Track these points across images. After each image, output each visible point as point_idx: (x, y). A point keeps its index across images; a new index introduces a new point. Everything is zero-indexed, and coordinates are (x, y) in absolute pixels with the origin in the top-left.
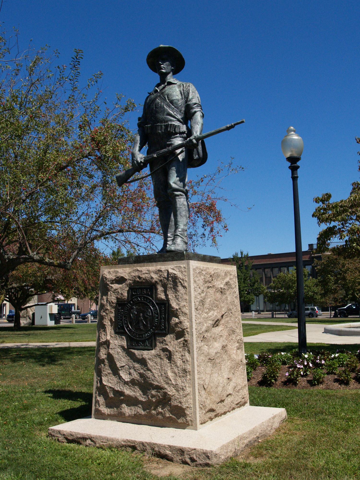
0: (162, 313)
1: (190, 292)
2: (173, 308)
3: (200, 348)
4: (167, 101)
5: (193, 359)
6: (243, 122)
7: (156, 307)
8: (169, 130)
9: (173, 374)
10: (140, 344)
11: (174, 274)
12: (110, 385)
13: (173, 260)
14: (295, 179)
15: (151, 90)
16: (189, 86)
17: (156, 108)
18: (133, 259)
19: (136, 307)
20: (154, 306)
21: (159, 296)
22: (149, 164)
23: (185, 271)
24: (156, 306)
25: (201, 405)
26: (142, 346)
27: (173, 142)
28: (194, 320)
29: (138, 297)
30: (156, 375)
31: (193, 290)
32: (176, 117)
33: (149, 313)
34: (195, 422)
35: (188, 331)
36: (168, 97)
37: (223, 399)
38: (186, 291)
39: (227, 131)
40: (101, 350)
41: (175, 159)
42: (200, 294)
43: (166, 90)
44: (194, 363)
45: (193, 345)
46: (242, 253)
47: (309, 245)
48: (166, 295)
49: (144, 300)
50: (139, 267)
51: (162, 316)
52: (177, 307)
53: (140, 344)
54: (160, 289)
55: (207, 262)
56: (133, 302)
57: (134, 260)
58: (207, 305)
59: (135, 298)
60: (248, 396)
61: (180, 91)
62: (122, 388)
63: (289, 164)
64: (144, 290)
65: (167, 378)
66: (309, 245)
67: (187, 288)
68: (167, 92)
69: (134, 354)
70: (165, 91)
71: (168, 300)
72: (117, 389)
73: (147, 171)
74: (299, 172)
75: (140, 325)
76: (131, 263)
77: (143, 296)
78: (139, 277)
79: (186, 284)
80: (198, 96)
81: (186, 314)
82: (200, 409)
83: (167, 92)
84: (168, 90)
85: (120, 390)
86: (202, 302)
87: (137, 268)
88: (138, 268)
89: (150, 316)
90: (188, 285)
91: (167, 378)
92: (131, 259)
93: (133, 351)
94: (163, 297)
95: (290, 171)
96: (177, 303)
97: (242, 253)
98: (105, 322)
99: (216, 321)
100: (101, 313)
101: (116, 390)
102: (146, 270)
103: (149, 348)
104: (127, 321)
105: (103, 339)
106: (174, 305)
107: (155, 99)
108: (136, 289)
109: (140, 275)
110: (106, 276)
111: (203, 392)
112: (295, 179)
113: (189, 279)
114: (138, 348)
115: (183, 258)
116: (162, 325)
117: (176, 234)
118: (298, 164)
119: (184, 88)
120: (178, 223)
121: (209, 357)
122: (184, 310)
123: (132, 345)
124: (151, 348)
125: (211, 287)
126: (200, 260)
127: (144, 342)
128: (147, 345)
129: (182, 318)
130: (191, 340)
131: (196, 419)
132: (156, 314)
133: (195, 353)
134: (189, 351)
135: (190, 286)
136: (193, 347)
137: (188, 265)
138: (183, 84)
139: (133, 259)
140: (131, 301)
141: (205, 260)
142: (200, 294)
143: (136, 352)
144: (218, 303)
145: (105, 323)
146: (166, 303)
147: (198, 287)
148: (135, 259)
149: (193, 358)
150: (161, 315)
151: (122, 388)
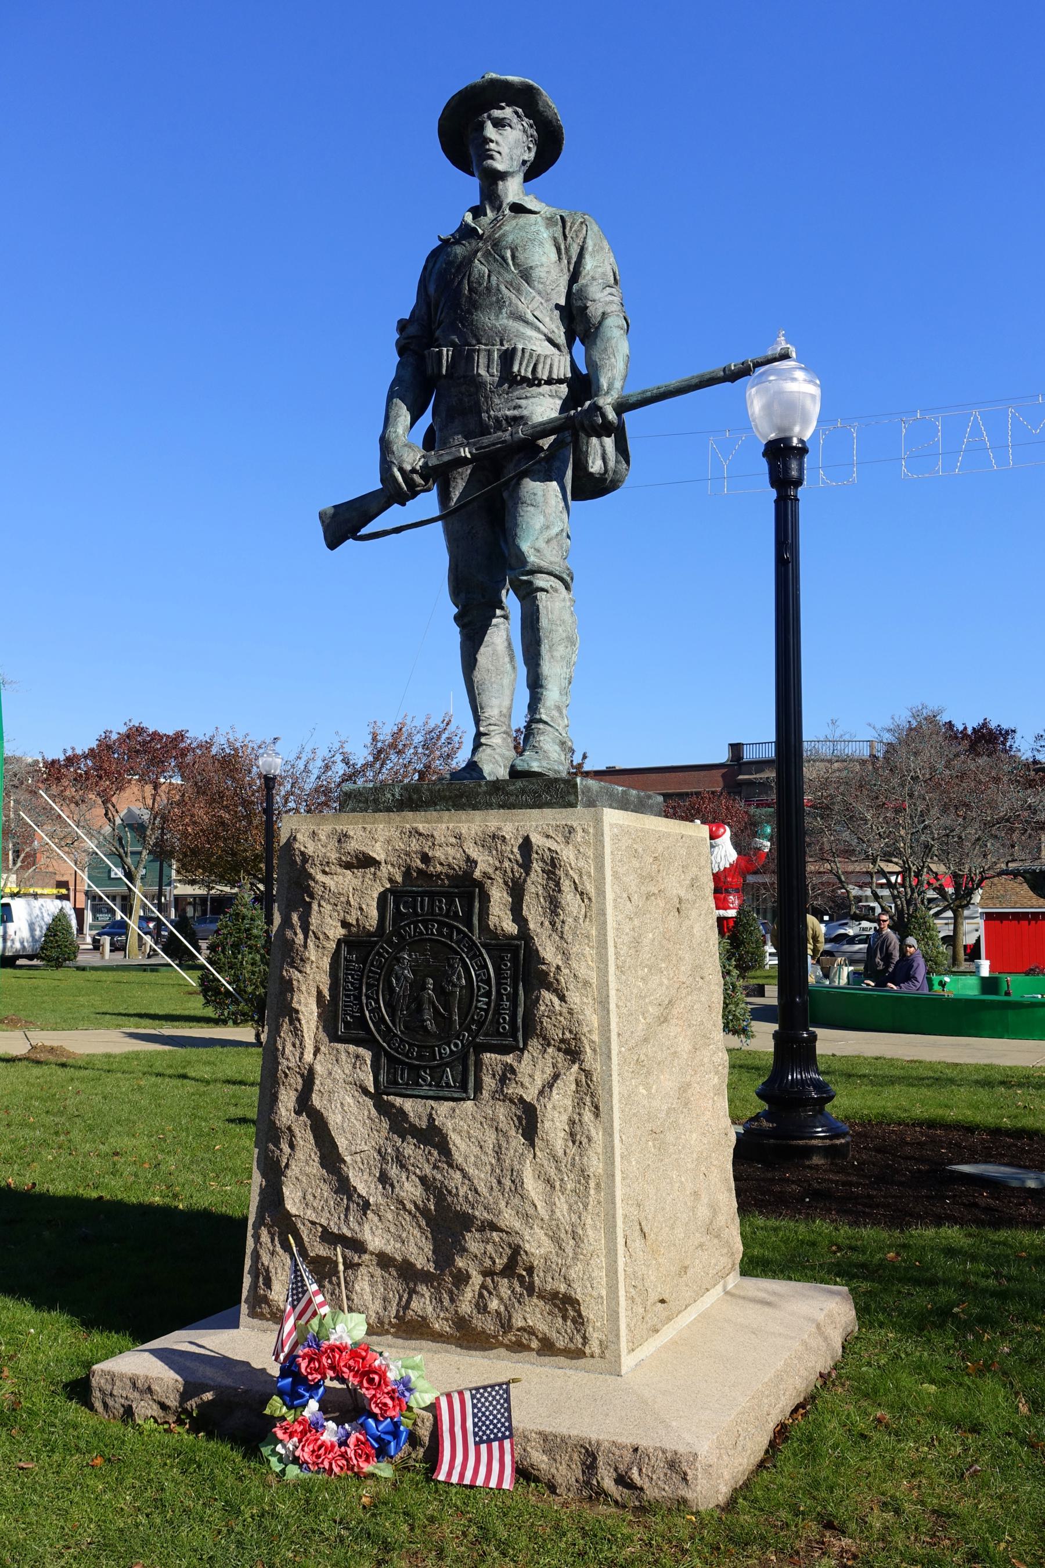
0: (506, 978)
1: (603, 913)
2: (544, 964)
3: (628, 1099)
4: (513, 268)
5: (611, 1135)
7: (484, 960)
8: (515, 369)
9: (541, 1186)
10: (424, 1080)
11: (549, 849)
12: (311, 1215)
13: (538, 804)
15: (448, 230)
16: (582, 223)
17: (470, 290)
18: (393, 795)
19: (410, 956)
20: (476, 955)
21: (492, 921)
23: (587, 843)
24: (481, 955)
25: (632, 1290)
26: (430, 1085)
27: (525, 413)
28: (612, 1007)
29: (420, 921)
30: (483, 1189)
31: (612, 904)
32: (540, 325)
33: (459, 978)
34: (612, 1347)
35: (593, 1042)
36: (513, 257)
38: (588, 907)
39: (728, 384)
40: (281, 1097)
41: (536, 467)
42: (631, 919)
44: (613, 1147)
45: (610, 1089)
46: (73, 749)
48: (518, 917)
49: (440, 933)
50: (422, 822)
51: (506, 990)
52: (558, 961)
53: (424, 1080)
54: (499, 897)
56: (401, 937)
57: (397, 796)
58: (645, 955)
59: (408, 925)
61: (555, 239)
62: (357, 1228)
64: (440, 902)
65: (63, 1065)
66: (731, 745)
67: (593, 899)
68: (510, 238)
69: (401, 1111)
70: (504, 235)
71: (525, 934)
72: (336, 1231)
73: (427, 503)
75: (426, 1017)
76: (389, 810)
77: (437, 922)
78: (425, 858)
79: (590, 888)
80: (612, 260)
81: (586, 983)
82: (630, 1301)
83: (510, 238)
84: (512, 228)
85: (349, 1234)
86: (636, 943)
87: (415, 825)
88: (421, 827)
89: (462, 988)
90: (597, 888)
91: (63, 1065)
92: (389, 796)
93: (398, 1101)
94: (510, 927)
96: (557, 948)
97: (73, 749)
98: (299, 1003)
100: (285, 973)
101: (332, 1233)
102: (449, 833)
103: (456, 1095)
104: (377, 1002)
105: (288, 1059)
106: (548, 951)
107: (469, 260)
108: (414, 895)
109: (426, 850)
110: (303, 849)
111: (637, 1244)
113: (600, 867)
114: (416, 1093)
115: (572, 798)
116: (504, 1019)
117: (538, 717)
119: (568, 228)
120: (544, 682)
121: (649, 1126)
122: (583, 972)
123: (396, 1083)
124: (464, 1095)
126: (614, 805)
127: (437, 1072)
128: (448, 1085)
129: (574, 997)
130: (602, 1071)
131: (618, 1336)
132: (482, 981)
133: (616, 1114)
134: (597, 1108)
135: (601, 892)
136: (611, 1096)
137: (598, 821)
138: (561, 217)
139: (393, 795)
140: (392, 934)
142: (631, 919)
143: (408, 1105)
145: (295, 1005)
146: (518, 947)
147: (625, 895)
148: (401, 795)
149: (609, 1133)
150: (499, 984)
151: (353, 1224)
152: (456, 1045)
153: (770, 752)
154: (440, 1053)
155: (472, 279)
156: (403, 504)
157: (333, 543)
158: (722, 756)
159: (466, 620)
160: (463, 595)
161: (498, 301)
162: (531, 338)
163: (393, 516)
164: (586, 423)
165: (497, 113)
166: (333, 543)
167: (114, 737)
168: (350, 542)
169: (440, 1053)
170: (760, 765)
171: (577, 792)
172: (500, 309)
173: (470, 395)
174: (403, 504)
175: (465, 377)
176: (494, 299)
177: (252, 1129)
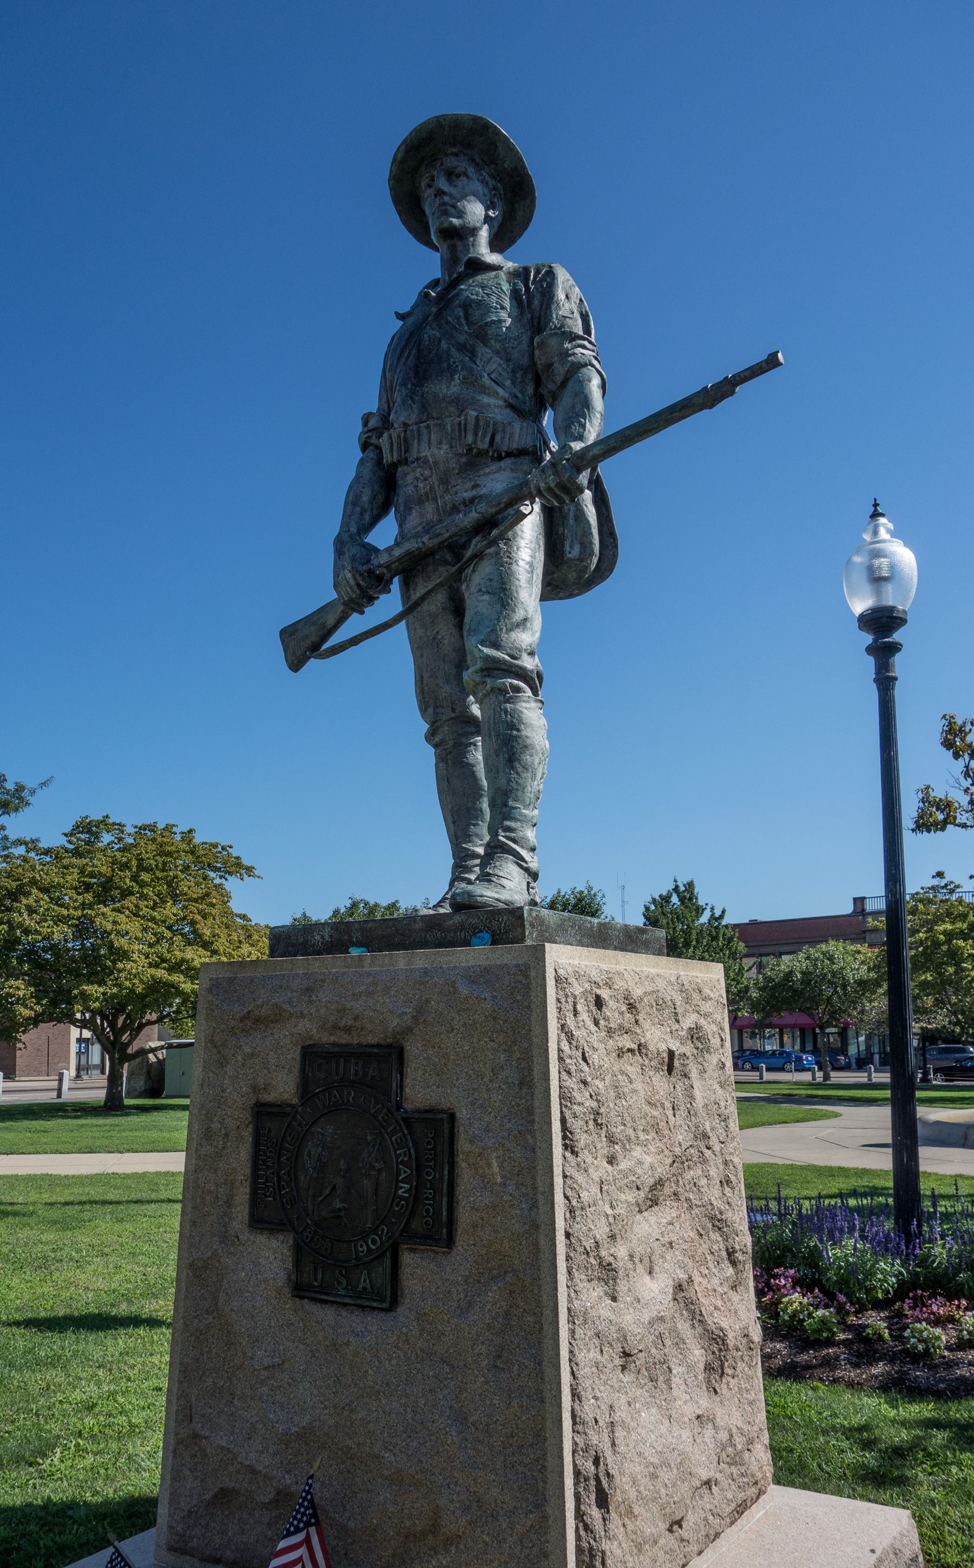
6: (771, 362)
14: (885, 683)
18: (323, 937)
22: (396, 580)
37: (678, 1518)
43: (509, 515)
47: (855, 900)
55: (615, 949)
57: (327, 938)
60: (772, 1470)
63: (868, 639)
66: (855, 900)
74: (899, 663)
95: (870, 661)
99: (653, 1188)
112: (885, 683)
118: (897, 636)
125: (630, 1050)
139: (323, 937)
141: (605, 940)
144: (656, 1113)
148: (331, 936)
152: (374, 1242)
153: (881, 905)
154: (356, 1251)
155: (422, 347)
156: (362, 613)
157: (296, 664)
158: (848, 909)
159: (437, 739)
160: (431, 710)
161: (449, 367)
162: (489, 405)
163: (355, 624)
164: (542, 485)
165: (450, 162)
166: (296, 664)
167: (343, 910)
168: (312, 662)
169: (356, 1251)
170: (875, 914)
171: (523, 925)
172: (452, 376)
173: (426, 479)
174: (362, 613)
175: (418, 459)
176: (445, 365)
177: (168, 1332)
